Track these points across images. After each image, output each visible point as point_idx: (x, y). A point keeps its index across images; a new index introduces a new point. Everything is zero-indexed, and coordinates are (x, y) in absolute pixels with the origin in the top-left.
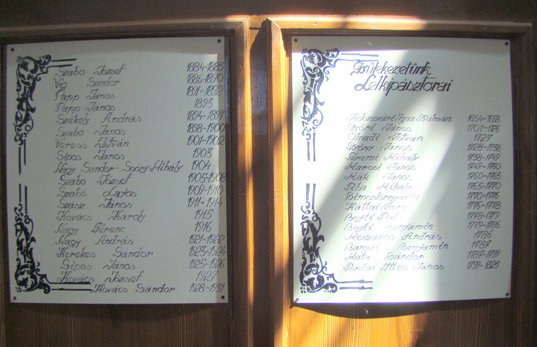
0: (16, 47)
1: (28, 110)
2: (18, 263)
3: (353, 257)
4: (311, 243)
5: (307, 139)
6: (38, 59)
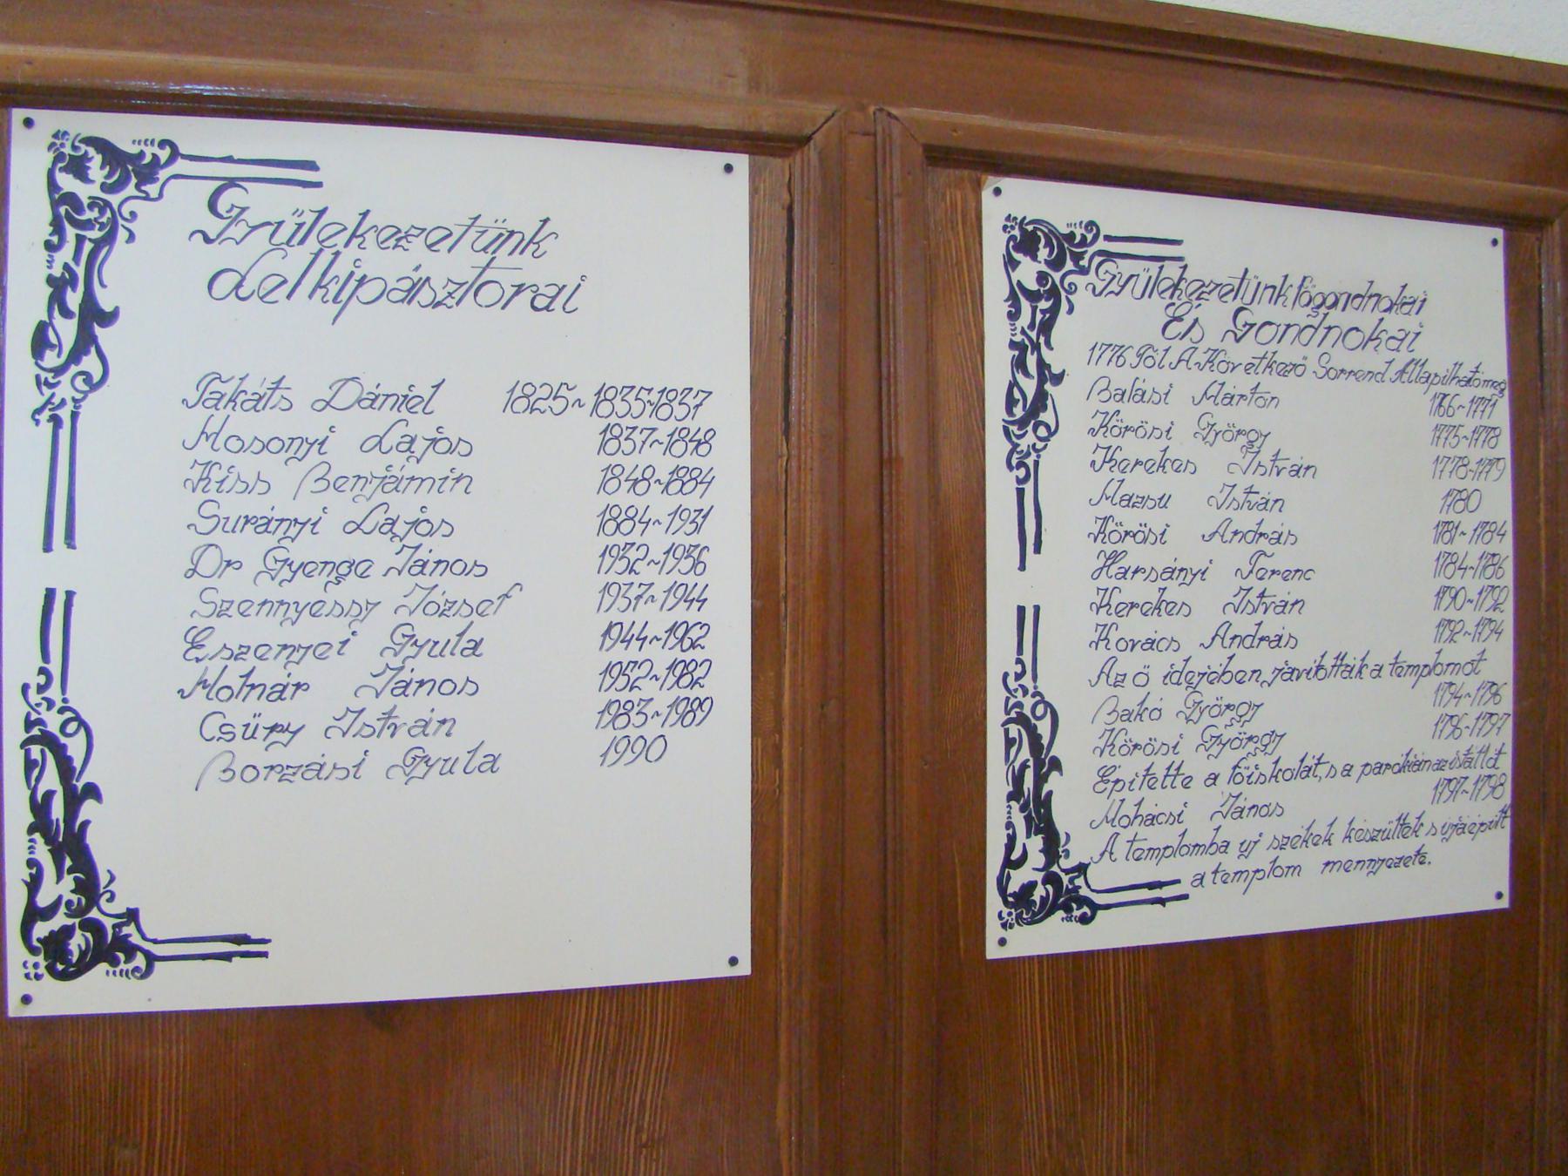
0: (1006, 183)
1: (1042, 381)
2: (31, 874)
3: (1113, 820)
4: (58, 810)
5: (1019, 481)
6: (1065, 230)
